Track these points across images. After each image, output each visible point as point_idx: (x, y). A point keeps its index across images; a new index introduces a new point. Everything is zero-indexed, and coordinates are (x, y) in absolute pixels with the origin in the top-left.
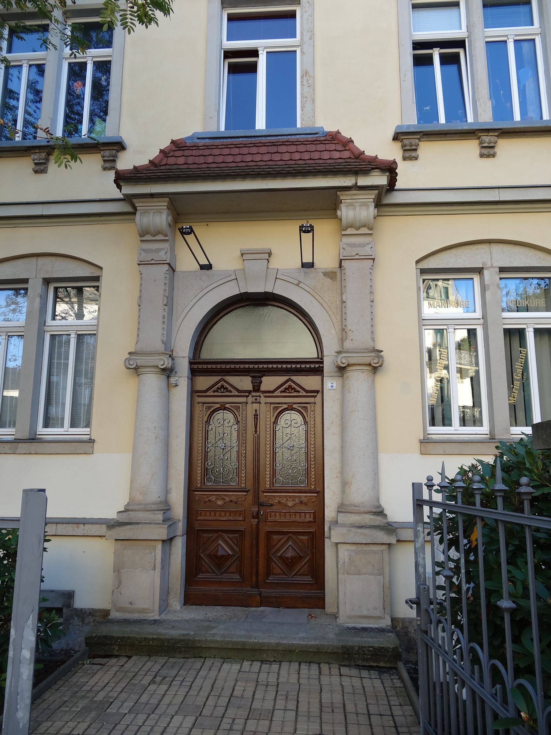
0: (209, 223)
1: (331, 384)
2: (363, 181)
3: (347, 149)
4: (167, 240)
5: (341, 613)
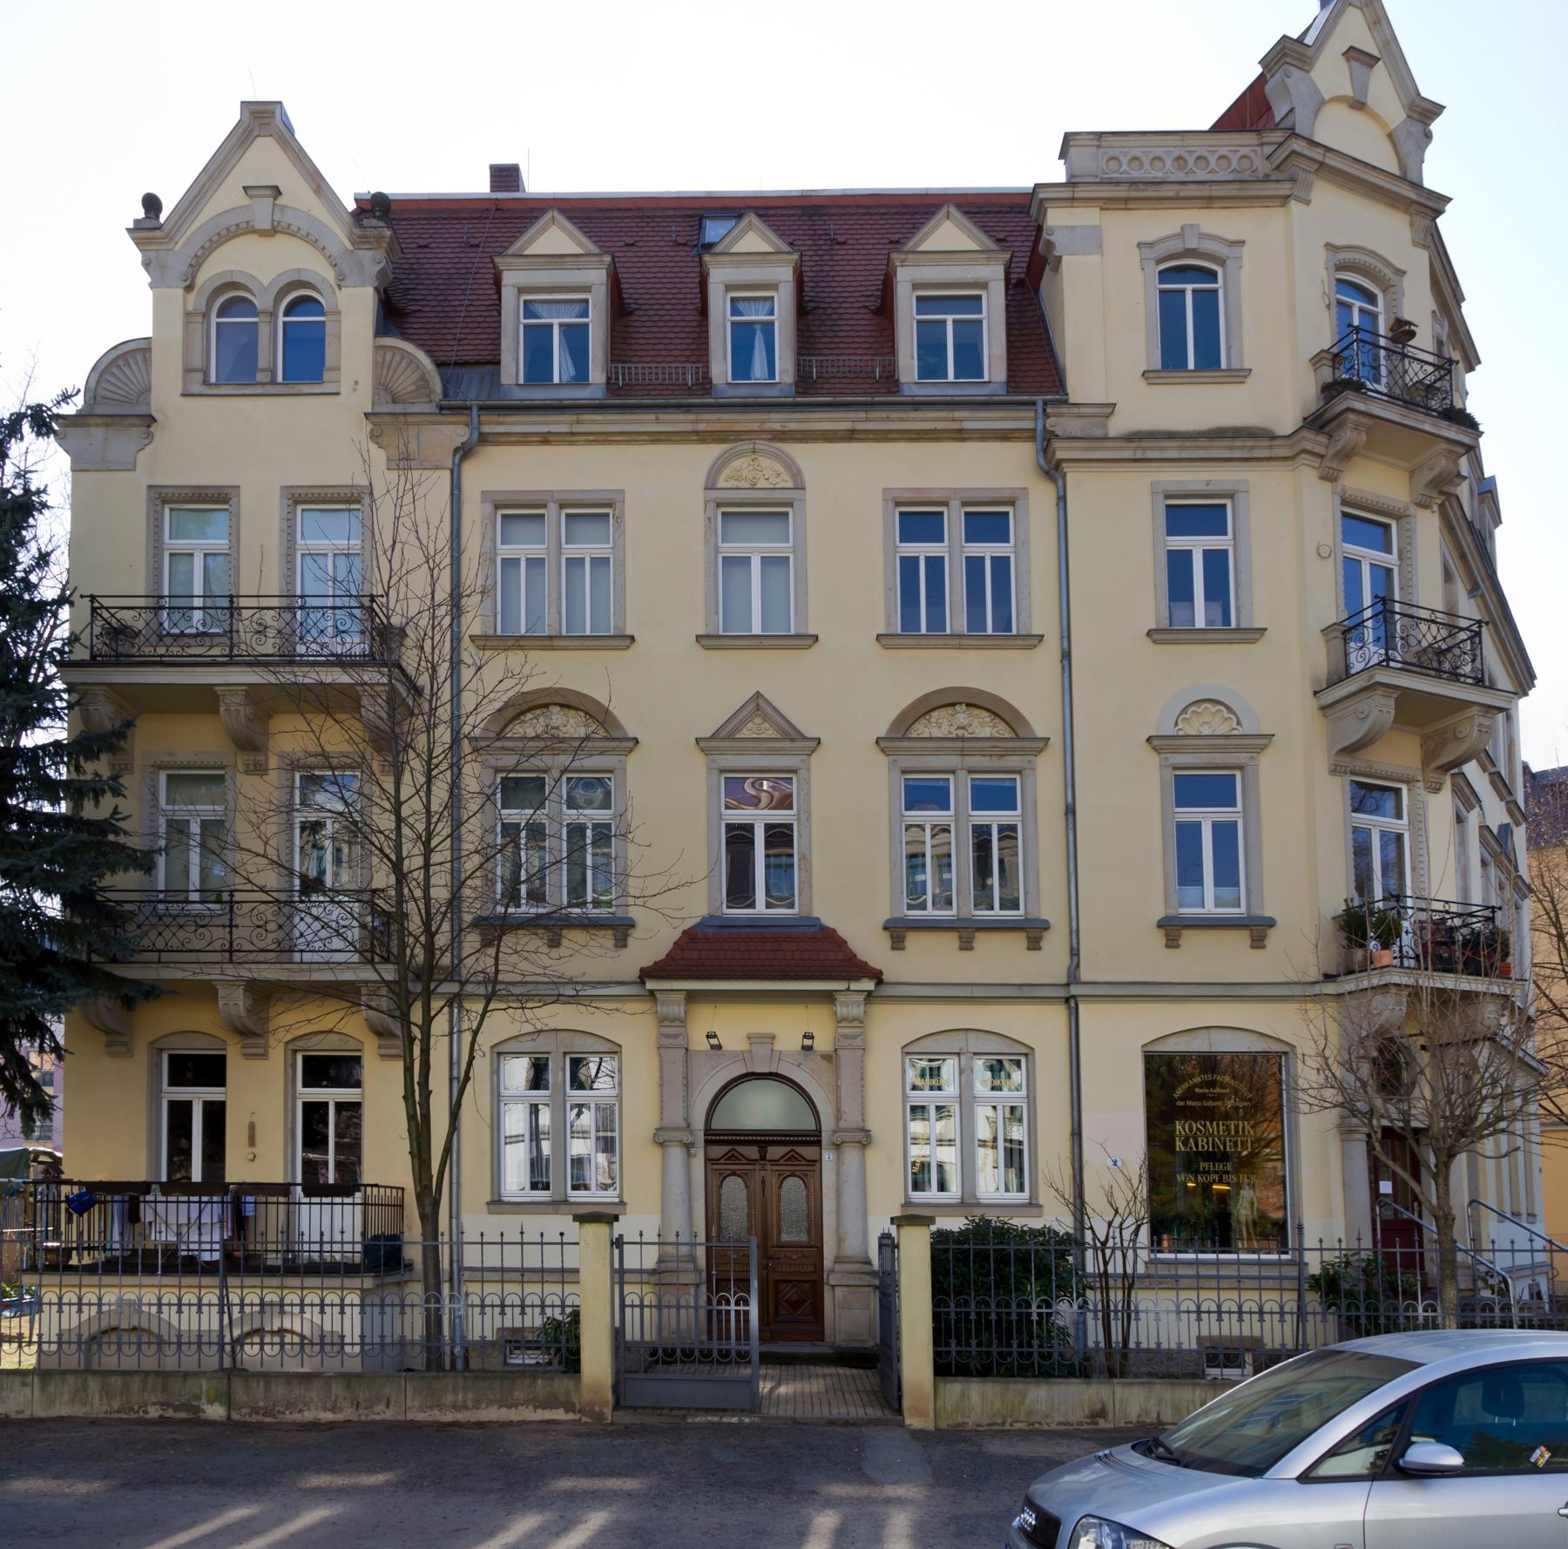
1: (828, 1156)
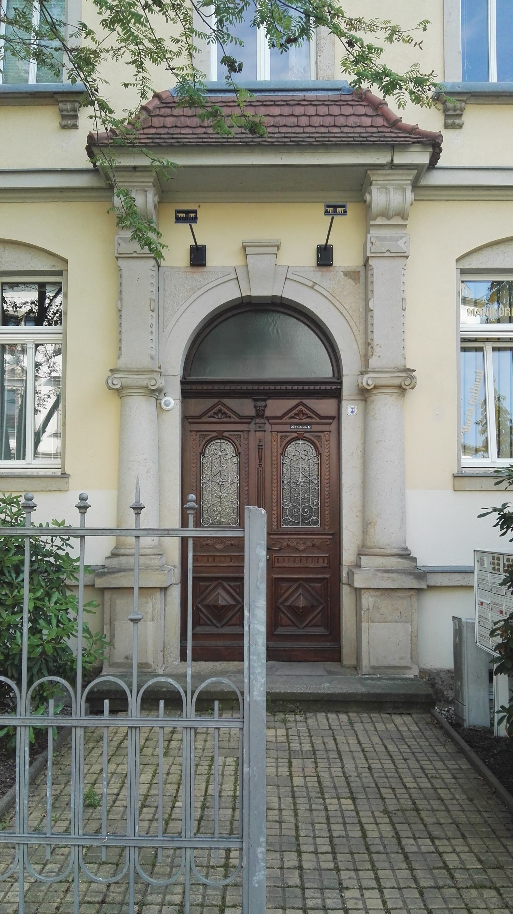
1: (350, 410)
2: (400, 159)
3: (379, 113)
5: (365, 662)
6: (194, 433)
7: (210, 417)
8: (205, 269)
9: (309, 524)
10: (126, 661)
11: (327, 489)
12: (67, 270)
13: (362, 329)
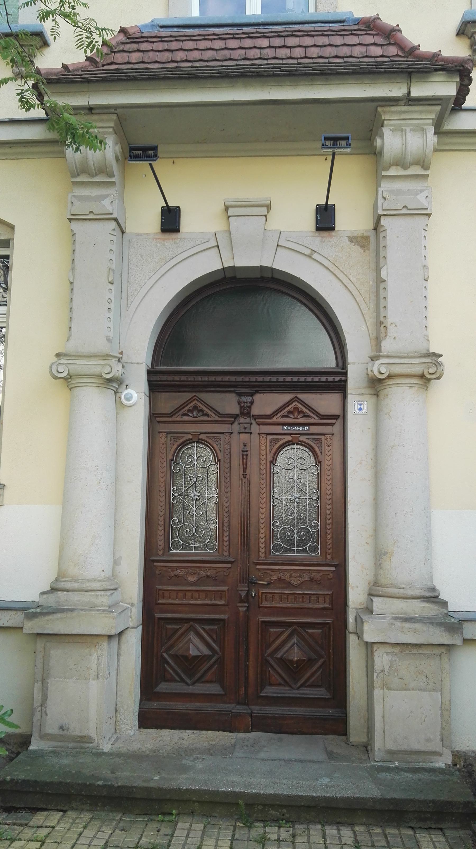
0: (175, 160)
1: (358, 406)
2: (418, 91)
3: (392, 41)
4: (113, 183)
5: (378, 744)
6: (163, 436)
7: (184, 415)
8: (179, 235)
9: (305, 551)
10: (61, 732)
11: (328, 507)
12: (13, 239)
13: (372, 305)
